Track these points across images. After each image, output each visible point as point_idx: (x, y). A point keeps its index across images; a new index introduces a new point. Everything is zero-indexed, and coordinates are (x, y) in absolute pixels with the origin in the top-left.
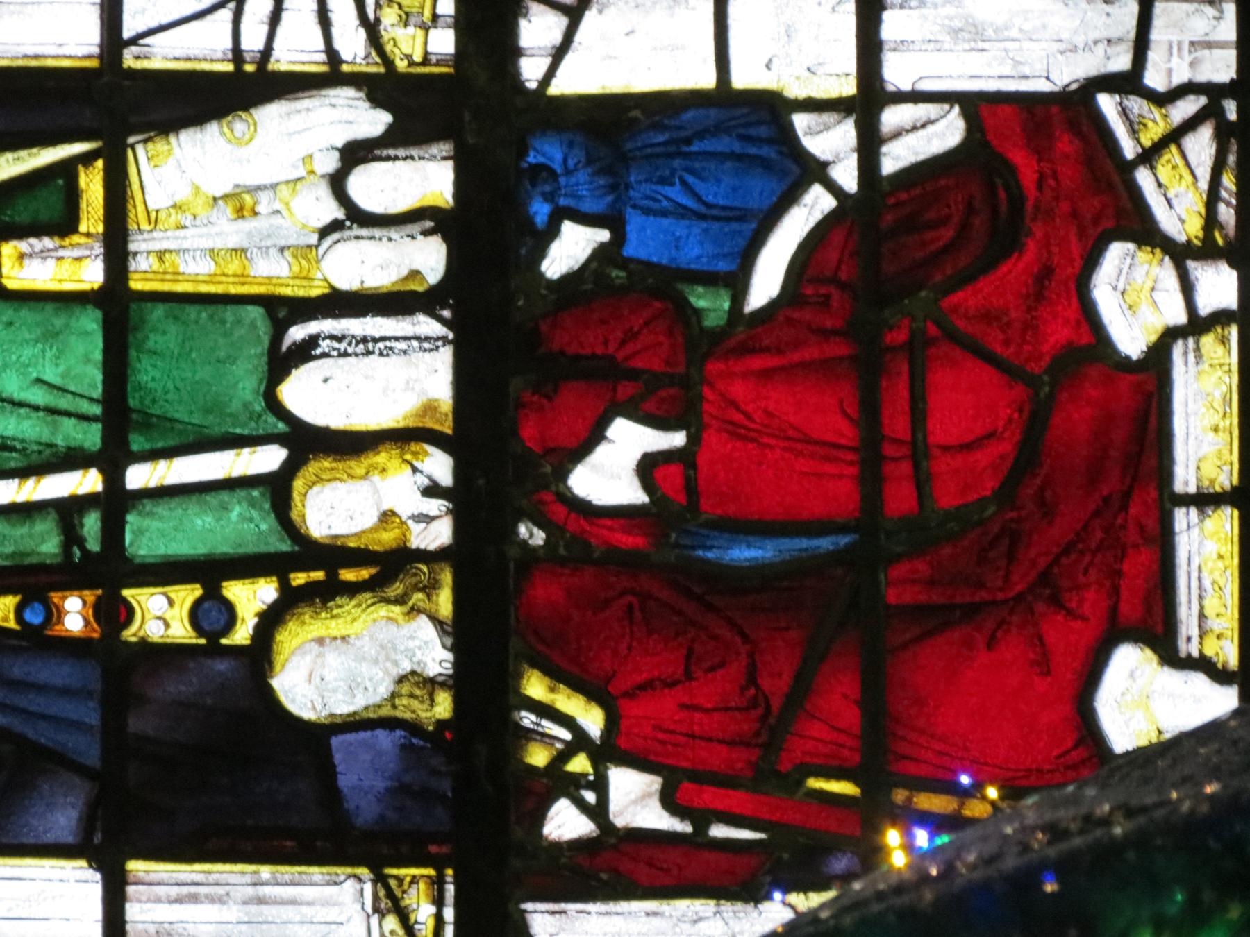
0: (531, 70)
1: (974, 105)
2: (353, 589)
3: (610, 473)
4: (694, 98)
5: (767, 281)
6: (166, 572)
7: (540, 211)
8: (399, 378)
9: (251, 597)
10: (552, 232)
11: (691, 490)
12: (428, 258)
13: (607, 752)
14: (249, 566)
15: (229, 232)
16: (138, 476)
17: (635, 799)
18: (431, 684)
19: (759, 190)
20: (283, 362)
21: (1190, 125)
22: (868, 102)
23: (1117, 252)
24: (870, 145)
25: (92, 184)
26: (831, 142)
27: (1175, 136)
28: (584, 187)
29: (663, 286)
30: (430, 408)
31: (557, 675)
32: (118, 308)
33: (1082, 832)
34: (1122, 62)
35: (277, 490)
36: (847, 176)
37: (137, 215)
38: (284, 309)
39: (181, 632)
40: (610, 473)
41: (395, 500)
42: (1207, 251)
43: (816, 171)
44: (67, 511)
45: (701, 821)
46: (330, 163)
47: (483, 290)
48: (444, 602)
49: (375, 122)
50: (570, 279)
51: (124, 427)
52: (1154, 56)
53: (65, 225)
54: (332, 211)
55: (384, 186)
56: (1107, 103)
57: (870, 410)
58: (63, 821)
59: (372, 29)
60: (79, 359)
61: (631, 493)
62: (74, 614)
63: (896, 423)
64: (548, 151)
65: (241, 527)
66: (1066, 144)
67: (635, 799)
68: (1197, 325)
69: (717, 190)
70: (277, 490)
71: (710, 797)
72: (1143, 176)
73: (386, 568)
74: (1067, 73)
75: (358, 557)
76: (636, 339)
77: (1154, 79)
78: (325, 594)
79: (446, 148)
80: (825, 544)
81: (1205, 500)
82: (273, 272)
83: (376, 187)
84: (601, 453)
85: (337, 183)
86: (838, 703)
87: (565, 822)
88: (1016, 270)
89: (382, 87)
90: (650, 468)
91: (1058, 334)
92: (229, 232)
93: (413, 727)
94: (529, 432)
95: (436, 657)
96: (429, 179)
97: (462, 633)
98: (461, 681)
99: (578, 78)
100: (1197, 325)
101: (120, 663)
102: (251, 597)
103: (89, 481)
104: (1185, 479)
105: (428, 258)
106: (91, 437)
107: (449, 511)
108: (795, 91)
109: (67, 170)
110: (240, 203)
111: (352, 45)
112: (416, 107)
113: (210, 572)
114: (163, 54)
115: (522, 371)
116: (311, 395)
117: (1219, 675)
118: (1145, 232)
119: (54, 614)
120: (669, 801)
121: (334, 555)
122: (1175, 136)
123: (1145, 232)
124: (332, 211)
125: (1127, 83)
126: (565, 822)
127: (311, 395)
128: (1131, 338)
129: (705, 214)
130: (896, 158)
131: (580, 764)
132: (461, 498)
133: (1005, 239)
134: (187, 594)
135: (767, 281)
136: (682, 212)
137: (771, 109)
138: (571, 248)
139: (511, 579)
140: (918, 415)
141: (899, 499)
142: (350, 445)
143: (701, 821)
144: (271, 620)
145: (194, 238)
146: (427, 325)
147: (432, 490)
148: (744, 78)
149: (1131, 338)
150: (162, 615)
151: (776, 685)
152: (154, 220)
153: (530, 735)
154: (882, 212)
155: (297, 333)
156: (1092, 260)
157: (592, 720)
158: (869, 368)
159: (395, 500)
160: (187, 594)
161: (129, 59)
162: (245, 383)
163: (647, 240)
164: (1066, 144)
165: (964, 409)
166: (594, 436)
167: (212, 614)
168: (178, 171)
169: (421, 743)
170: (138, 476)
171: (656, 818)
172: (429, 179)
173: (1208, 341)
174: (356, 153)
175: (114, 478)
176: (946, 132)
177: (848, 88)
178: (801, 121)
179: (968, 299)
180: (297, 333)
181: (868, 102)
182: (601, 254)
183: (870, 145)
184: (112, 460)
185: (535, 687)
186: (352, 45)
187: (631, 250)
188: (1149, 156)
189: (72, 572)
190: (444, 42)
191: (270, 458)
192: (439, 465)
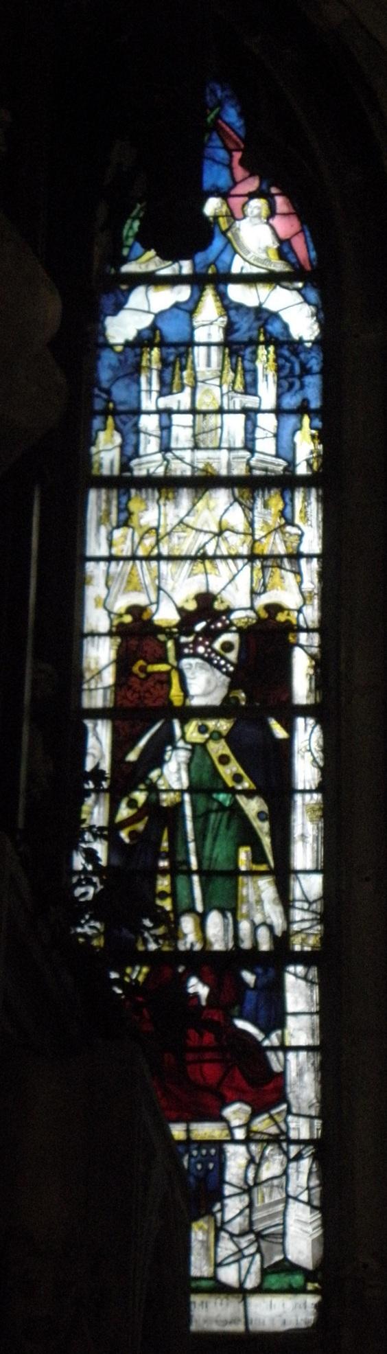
0: (291, 969)
1: (283, 1075)
3: (198, 988)
5: (241, 1024)
6: (173, 884)
12: (246, 945)
14: (174, 903)
15: (252, 898)
16: (196, 878)
20: (222, 911)
21: (279, 1127)
23: (248, 1109)
25: (263, 868)
26: (274, 1039)
27: (276, 1124)
28: (264, 980)
29: (240, 1001)
30: (211, 944)
34: (294, 1110)
35: (191, 910)
36: (266, 1043)
37: (255, 878)
43: (267, 1036)
44: (188, 863)
46: (268, 921)
47: (238, 957)
49: (278, 932)
51: (207, 875)
52: (296, 1119)
56: (284, 1107)
60: (222, 864)
62: (164, 864)
63: (207, 1056)
65: (184, 902)
66: (275, 1096)
70: (191, 910)
72: (266, 1116)
74: (291, 1097)
76: (228, 995)
77: (290, 1118)
79: (194, 1327)
81: (188, 1131)
85: (264, 924)
88: (244, 1084)
89: (287, 934)
90: (196, 996)
91: (228, 1094)
94: (206, 969)
96: (265, 946)
99: (289, 979)
106: (205, 867)
107: (319, 1186)
108: (287, 1032)
109: (266, 861)
110: (260, 901)
111: (295, 927)
112: (282, 941)
113: (173, 894)
115: (220, 966)
116: (214, 919)
118: (254, 1115)
119: (164, 859)
122: (276, 1124)
125: (289, 1112)
127: (214, 919)
129: (257, 1009)
130: (271, 1056)
132: (190, 953)
134: (168, 890)
135: (241, 1024)
136: (257, 1004)
137: (281, 1025)
138: (249, 977)
140: (210, 1061)
146: (231, 945)
147: (192, 945)
149: (228, 1112)
150: (164, 884)
152: (256, 882)
153: (133, 970)
154: (257, 1052)
155: (229, 915)
156: (247, 1103)
160: (168, 890)
162: (216, 903)
163: (251, 995)
164: (275, 1096)
165: (211, 1072)
167: (163, 895)
168: (266, 888)
169: (21, 825)
170: (196, 878)
173: (227, 1132)
174: (271, 928)
176: (277, 1067)
177: (287, 1044)
178: (279, 1032)
179: (237, 1073)
181: (284, 1048)
185: (145, 970)
186: (295, 927)
188: (271, 1117)
190: (297, 948)
191: (199, 907)
192: (198, 947)
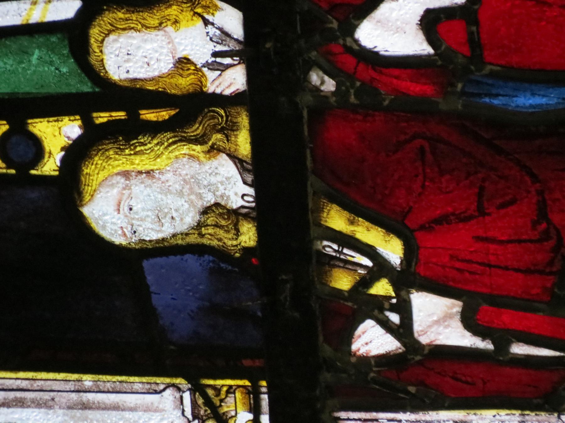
2: (154, 129)
9: (57, 134)
11: (474, 43)
13: (407, 279)
14: (55, 106)
17: (437, 319)
18: (235, 216)
48: (243, 143)
58: (349, 41)
61: (415, 45)
67: (437, 319)
71: (507, 318)
73: (186, 112)
78: (129, 133)
87: (372, 340)
95: (237, 191)
98: (262, 212)
120: (470, 322)
121: (134, 96)
126: (372, 340)
131: (382, 288)
144: (77, 155)
157: (393, 251)
171: (458, 337)
185: (337, 220)
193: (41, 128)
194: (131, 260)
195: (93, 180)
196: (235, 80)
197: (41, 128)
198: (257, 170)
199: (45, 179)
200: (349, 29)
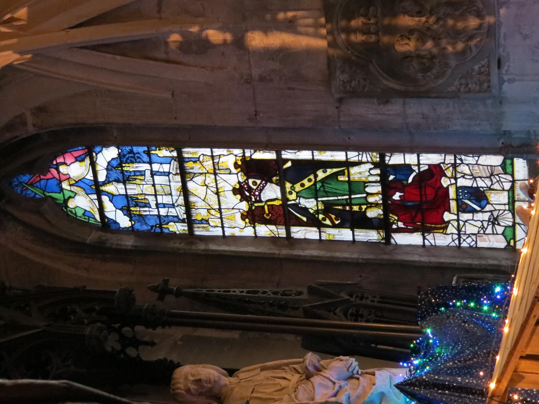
0: (387, 162)
1: (429, 165)
2: (373, 207)
3: (397, 196)
4: (402, 165)
5: (410, 180)
7: (388, 174)
8: (377, 188)
9: (364, 207)
10: (389, 176)
11: (404, 199)
13: (398, 221)
14: (364, 204)
15: (359, 176)
17: (401, 224)
18: (381, 215)
19: (409, 173)
22: (419, 165)
23: (443, 178)
24: (419, 168)
25: (346, 171)
26: (416, 168)
27: (448, 168)
31: (393, 214)
32: (349, 182)
33: (282, 295)
34: (443, 161)
35: (365, 198)
36: (417, 171)
37: (350, 174)
38: (365, 182)
39: (358, 210)
40: (397, 196)
41: (377, 199)
42: (452, 178)
43: (414, 171)
44: (346, 199)
45: (407, 226)
46: (368, 170)
47: (383, 181)
48: (382, 208)
50: (392, 180)
51: (351, 192)
53: (344, 174)
54: (369, 174)
55: (373, 172)
56: (442, 165)
57: (421, 192)
58: (348, 226)
59: (371, 158)
60: (346, 186)
61: (399, 199)
62: (348, 208)
63: (423, 193)
64: (389, 169)
65: (363, 201)
67: (401, 224)
68: (451, 184)
69: (405, 172)
70: (365, 198)
71: (408, 224)
72: (445, 171)
73: (376, 205)
74: (438, 162)
75: (374, 204)
77: (446, 163)
78: (371, 207)
80: (417, 203)
82: (364, 179)
83: (372, 172)
84: (395, 195)
85: (369, 172)
86: (419, 217)
87: (394, 226)
89: (373, 163)
90: (400, 196)
92: (359, 176)
93: (380, 219)
95: (381, 213)
96: (378, 171)
97: (383, 210)
98: (384, 214)
100: (451, 184)
101: (351, 212)
102: (364, 207)
103: (347, 197)
104: (451, 197)
105: (378, 178)
109: (344, 170)
110: (360, 173)
111: (370, 160)
113: (360, 205)
114: (352, 160)
115: (387, 189)
116: (368, 190)
117: (455, 214)
118: (446, 176)
120: (404, 225)
121: (371, 203)
122: (448, 168)
123: (446, 176)
124: (369, 174)
125: (444, 163)
126: (394, 226)
127: (368, 190)
128: (445, 185)
129: (404, 175)
130: (421, 170)
131: (395, 222)
133: (433, 177)
134: (358, 207)
135: (410, 180)
138: (391, 177)
139: (388, 206)
140: (425, 192)
141: (424, 199)
142: (372, 194)
143: (407, 226)
144: (366, 209)
145: (356, 176)
146: (378, 184)
148: (407, 162)
149: (445, 185)
150: (356, 208)
151: (414, 215)
154: (421, 174)
155: (366, 185)
157: (396, 218)
158: (420, 188)
159: (377, 199)
161: (349, 160)
163: (399, 177)
164: (438, 169)
165: (430, 193)
166: (395, 194)
167: (360, 208)
168: (354, 170)
170: (353, 196)
171: (403, 226)
172: (378, 171)
174: (371, 169)
175: (350, 197)
176: (426, 167)
180: (366, 185)
181: (419, 165)
182: (394, 178)
183: (419, 168)
184: (350, 195)
185: (391, 215)
186: (370, 160)
187: (397, 177)
188: (446, 169)
189: (347, 205)
190: (378, 159)
191: (365, 195)
192: (381, 196)
193: (362, 206)
194: (371, 219)
195: (163, 292)
196: (381, 202)
197: (362, 206)
198: (383, 210)
199: (307, 220)
200: (392, 197)
